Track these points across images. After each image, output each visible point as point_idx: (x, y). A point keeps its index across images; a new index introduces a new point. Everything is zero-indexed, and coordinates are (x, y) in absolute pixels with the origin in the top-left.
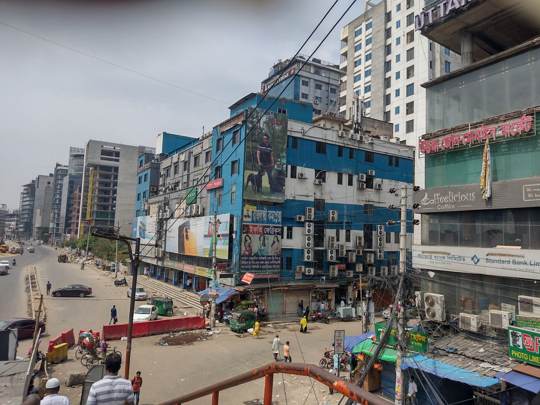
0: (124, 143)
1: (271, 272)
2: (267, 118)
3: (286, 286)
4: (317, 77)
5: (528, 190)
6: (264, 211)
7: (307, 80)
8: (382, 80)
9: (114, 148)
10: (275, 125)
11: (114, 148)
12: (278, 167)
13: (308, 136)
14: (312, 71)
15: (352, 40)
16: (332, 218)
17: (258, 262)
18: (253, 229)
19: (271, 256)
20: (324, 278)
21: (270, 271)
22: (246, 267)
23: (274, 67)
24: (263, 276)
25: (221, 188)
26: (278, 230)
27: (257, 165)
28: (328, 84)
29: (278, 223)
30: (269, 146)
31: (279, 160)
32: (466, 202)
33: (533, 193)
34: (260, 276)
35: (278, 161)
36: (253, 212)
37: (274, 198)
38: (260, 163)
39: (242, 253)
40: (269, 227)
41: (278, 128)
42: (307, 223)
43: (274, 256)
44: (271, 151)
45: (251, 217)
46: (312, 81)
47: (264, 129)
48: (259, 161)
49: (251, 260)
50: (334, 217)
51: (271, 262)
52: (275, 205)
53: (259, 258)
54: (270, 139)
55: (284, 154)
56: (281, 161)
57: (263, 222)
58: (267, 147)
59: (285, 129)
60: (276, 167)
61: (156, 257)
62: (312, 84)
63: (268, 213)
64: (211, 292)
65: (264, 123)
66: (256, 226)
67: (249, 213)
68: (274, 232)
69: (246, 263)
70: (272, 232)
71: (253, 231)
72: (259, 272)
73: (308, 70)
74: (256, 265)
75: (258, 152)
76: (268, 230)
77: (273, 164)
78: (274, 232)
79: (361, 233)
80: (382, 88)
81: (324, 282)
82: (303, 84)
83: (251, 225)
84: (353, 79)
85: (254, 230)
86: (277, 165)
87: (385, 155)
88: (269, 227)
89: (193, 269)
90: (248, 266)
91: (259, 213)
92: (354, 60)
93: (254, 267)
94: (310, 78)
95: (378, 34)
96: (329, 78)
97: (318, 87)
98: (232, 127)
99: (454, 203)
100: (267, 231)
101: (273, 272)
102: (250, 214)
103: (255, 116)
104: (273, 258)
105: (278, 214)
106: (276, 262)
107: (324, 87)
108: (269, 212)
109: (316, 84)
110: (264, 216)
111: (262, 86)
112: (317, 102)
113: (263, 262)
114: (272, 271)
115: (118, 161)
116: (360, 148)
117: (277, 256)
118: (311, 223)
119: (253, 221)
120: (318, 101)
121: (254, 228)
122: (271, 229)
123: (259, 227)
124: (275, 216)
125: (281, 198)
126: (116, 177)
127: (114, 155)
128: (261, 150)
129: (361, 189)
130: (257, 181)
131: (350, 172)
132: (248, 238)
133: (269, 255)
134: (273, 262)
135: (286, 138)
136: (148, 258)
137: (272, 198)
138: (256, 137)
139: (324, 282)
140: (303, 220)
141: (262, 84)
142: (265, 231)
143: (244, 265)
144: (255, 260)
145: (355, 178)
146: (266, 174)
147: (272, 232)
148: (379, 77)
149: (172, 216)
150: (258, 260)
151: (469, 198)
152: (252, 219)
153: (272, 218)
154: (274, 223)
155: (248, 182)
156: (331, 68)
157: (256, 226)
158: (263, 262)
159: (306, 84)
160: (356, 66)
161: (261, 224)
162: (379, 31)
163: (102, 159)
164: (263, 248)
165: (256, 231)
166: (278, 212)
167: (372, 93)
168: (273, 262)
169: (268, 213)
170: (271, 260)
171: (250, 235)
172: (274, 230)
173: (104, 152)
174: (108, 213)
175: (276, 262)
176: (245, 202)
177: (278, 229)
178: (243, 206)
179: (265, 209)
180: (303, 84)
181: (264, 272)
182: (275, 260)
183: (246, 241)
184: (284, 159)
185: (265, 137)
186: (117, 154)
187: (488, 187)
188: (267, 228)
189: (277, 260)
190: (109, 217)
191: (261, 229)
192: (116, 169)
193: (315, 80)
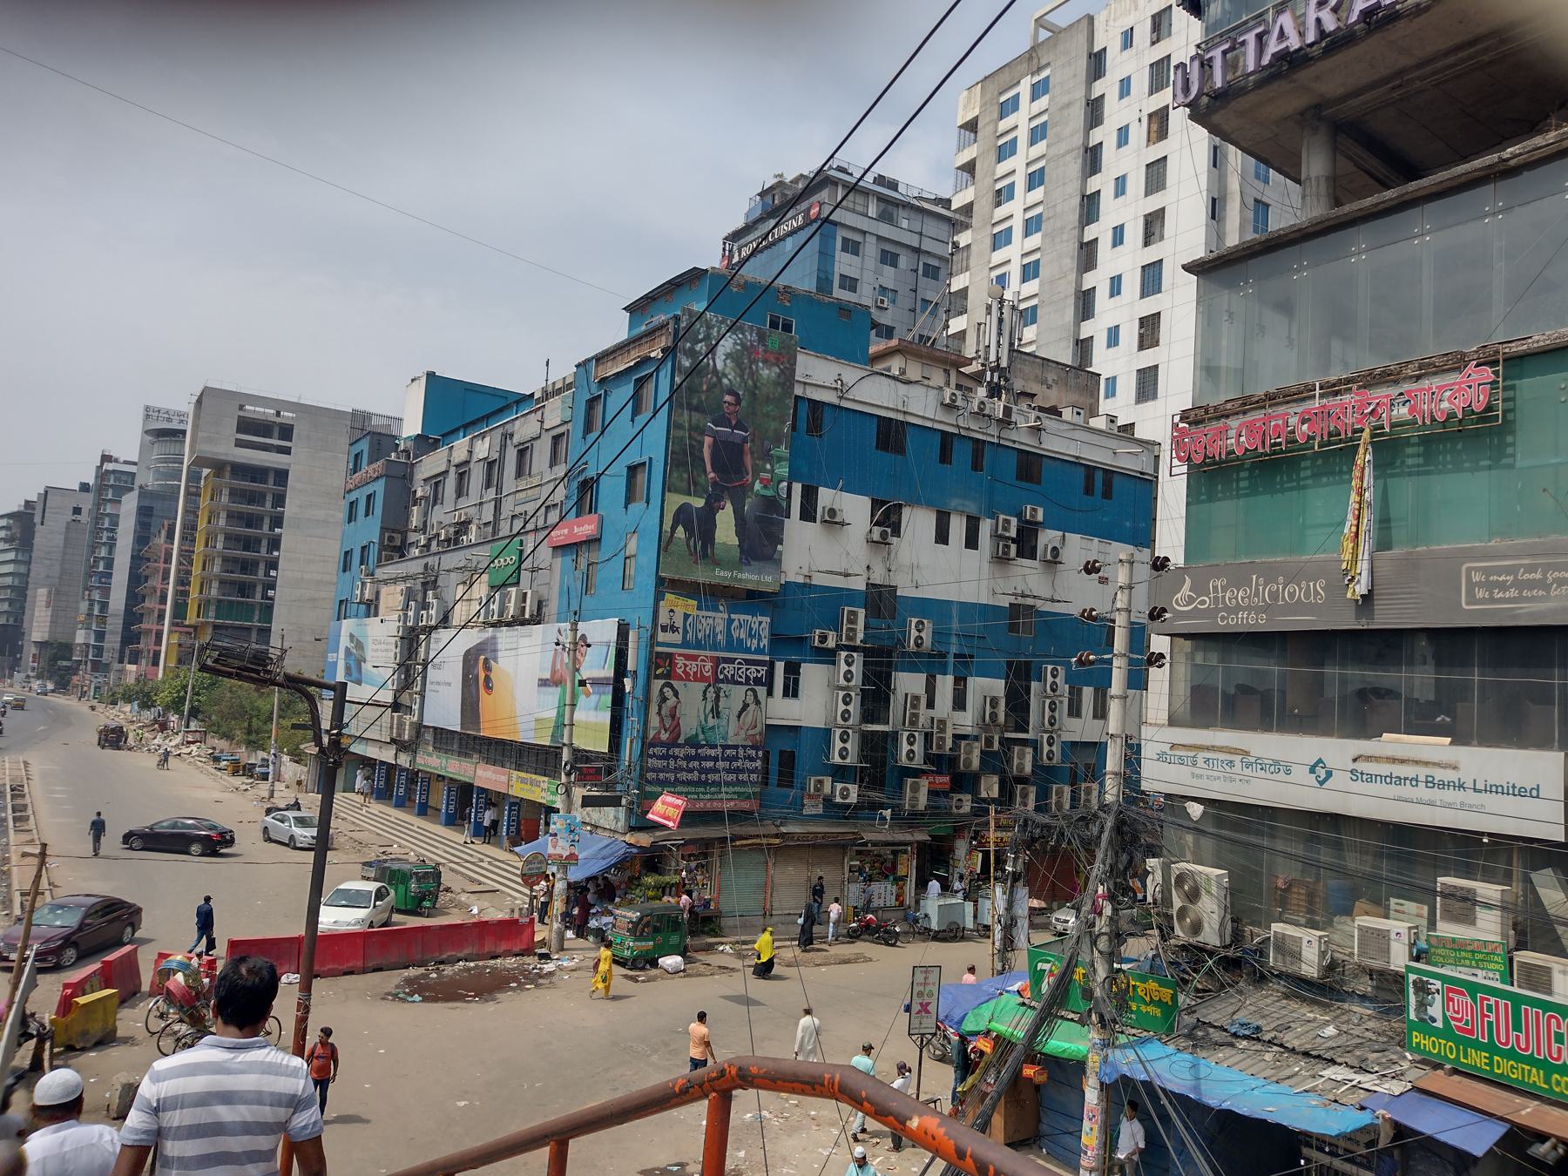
0: (308, 400)
1: (734, 793)
2: (735, 343)
3: (777, 836)
4: (885, 230)
5: (1476, 578)
6: (720, 615)
7: (857, 238)
8: (1073, 247)
9: (278, 414)
10: (760, 364)
11: (278, 414)
12: (765, 487)
13: (854, 400)
14: (873, 210)
15: (991, 128)
16: (916, 642)
17: (696, 764)
18: (686, 665)
19: (736, 747)
20: (887, 813)
21: (731, 789)
22: (661, 776)
23: (762, 194)
24: (708, 805)
25: (593, 542)
26: (758, 671)
27: (702, 480)
28: (917, 251)
29: (759, 651)
30: (740, 426)
31: (768, 466)
32: (1298, 607)
33: (1490, 586)
34: (702, 805)
35: (765, 471)
36: (686, 616)
37: (750, 578)
38: (712, 475)
39: (652, 734)
40: (732, 661)
41: (767, 373)
42: (844, 654)
43: (744, 747)
44: (745, 440)
45: (681, 630)
46: (871, 240)
47: (725, 375)
48: (709, 468)
49: (676, 758)
50: (921, 638)
51: (735, 764)
52: (752, 599)
53: (699, 751)
54: (744, 403)
55: (783, 450)
56: (772, 471)
57: (715, 647)
58: (733, 428)
59: (788, 377)
60: (757, 486)
61: (393, 741)
62: (871, 248)
63: (730, 621)
64: (554, 847)
65: (728, 356)
66: (694, 658)
67: (674, 619)
68: (748, 678)
69: (660, 763)
70: (740, 677)
71: (685, 672)
72: (698, 794)
73: (859, 208)
74: (691, 771)
75: (708, 440)
76: (729, 669)
77: (750, 477)
78: (748, 678)
79: (998, 686)
80: (1072, 269)
81: (887, 826)
82: (844, 249)
83: (680, 655)
84: (988, 242)
85: (688, 669)
86: (762, 481)
87: (1076, 463)
88: (732, 661)
89: (504, 779)
90: (667, 775)
91: (703, 620)
92: (994, 186)
93: (683, 776)
94: (864, 233)
95: (1066, 112)
96: (921, 234)
97: (888, 258)
98: (632, 364)
99: (1266, 609)
100: (726, 672)
101: (739, 794)
102: (679, 623)
103: (700, 337)
104: (741, 751)
105: (760, 623)
106: (748, 764)
107: (904, 261)
108: (733, 616)
109: (882, 250)
110: (718, 630)
111: (724, 249)
112: (882, 302)
113: (709, 764)
114: (737, 789)
115: (287, 451)
116: (1002, 442)
117: (752, 747)
118: (855, 654)
119: (685, 644)
120: (886, 300)
121: (687, 663)
122: (739, 669)
123: (703, 660)
124: (751, 629)
125: (769, 579)
126: (280, 500)
127: (276, 432)
128: (715, 435)
129: (1001, 559)
130: (700, 526)
131: (972, 508)
132: (668, 692)
133: (730, 743)
134: (739, 763)
135: (791, 402)
136: (369, 742)
137: (745, 576)
138: (703, 398)
139: (887, 826)
140: (831, 643)
141: (724, 243)
142: (721, 673)
143: (653, 770)
144: (688, 758)
145: (986, 527)
146: (729, 507)
147: (740, 677)
148: (1065, 237)
149: (445, 621)
150: (697, 757)
151: (1307, 595)
152: (684, 637)
153: (743, 636)
154: (748, 651)
155: (673, 529)
156: (926, 206)
157: (694, 658)
158: (709, 764)
159: (852, 247)
160: (999, 204)
161: (708, 653)
162: (1068, 105)
163: (240, 444)
164: (711, 722)
165: (695, 673)
166: (760, 618)
167: (1041, 284)
168: (739, 763)
169: (730, 621)
170: (736, 758)
171: (675, 683)
172: (747, 669)
173: (246, 425)
174: (252, 605)
175: (748, 764)
176: (664, 585)
177: (759, 668)
178: (659, 597)
179: (721, 608)
180: (844, 249)
181: (713, 794)
182: (745, 758)
183: (664, 699)
184: (783, 463)
185: (728, 398)
186: (286, 432)
187: (1363, 567)
188: (726, 666)
189: (752, 759)
190: (256, 618)
191: (709, 665)
192: (282, 476)
193: (880, 238)
